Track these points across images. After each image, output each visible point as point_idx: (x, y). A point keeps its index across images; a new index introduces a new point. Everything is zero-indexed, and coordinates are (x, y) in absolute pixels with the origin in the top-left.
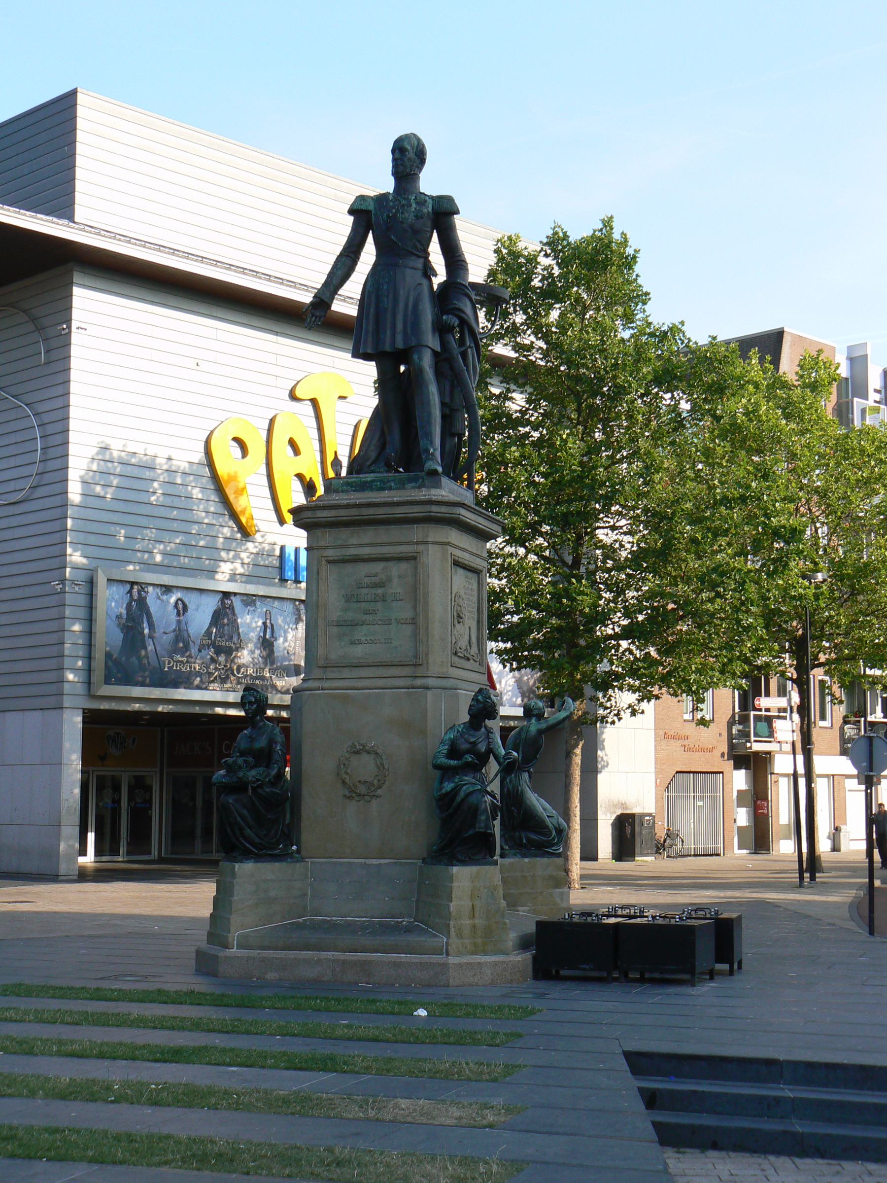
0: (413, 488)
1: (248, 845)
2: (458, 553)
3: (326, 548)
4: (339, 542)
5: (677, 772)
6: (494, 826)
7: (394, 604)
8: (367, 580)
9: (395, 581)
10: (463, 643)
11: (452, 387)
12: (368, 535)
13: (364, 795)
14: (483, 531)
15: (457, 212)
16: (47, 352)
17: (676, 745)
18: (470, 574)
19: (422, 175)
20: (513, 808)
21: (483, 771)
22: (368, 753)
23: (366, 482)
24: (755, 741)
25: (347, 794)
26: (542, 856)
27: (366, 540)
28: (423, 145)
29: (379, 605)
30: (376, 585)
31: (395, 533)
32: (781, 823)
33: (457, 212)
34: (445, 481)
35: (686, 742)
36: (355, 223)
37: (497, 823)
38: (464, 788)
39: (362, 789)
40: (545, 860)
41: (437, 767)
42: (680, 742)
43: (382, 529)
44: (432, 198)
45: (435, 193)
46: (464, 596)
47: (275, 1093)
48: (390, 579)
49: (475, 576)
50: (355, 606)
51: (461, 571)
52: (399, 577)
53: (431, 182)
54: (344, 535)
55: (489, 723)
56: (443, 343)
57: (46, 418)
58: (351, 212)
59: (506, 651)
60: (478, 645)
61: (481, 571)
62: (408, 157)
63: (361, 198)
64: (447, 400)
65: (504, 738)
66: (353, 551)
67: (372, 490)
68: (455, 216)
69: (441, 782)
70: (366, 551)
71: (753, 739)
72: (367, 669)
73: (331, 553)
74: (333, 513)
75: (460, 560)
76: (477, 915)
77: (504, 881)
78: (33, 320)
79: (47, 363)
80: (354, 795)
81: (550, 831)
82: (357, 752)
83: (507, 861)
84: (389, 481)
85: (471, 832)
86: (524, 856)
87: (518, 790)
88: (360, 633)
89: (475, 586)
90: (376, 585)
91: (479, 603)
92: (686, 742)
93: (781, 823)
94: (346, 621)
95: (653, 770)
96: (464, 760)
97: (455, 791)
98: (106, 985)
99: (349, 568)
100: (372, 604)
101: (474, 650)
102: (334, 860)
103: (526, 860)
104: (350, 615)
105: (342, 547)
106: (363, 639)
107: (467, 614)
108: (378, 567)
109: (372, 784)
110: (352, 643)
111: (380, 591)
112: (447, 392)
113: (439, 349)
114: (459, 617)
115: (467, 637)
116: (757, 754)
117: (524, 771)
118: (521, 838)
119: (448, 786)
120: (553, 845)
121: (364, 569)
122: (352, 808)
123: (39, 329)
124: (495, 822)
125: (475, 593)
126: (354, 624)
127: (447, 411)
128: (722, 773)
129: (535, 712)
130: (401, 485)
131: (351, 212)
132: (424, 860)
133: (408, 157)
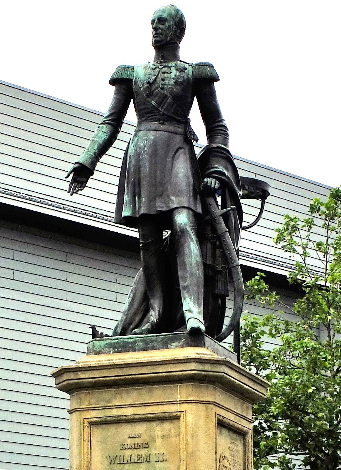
0: (176, 347)
2: (223, 413)
4: (102, 404)
8: (129, 442)
9: (159, 442)
14: (248, 391)
15: (217, 79)
23: (128, 343)
27: (129, 402)
30: (138, 447)
31: (159, 394)
32: (258, 273)
33: (217, 79)
34: (208, 340)
36: (117, 92)
43: (145, 390)
47: (181, 343)
48: (153, 439)
49: (239, 438)
51: (225, 432)
52: (164, 437)
54: (106, 395)
56: (206, 207)
58: (113, 82)
59: (221, 251)
61: (247, 433)
62: (169, 33)
64: (209, 262)
66: (115, 412)
67: (134, 350)
68: (215, 84)
70: (129, 412)
73: (93, 415)
74: (96, 374)
75: (225, 420)
84: (152, 341)
90: (138, 447)
93: (258, 273)
99: (112, 429)
105: (104, 408)
108: (141, 428)
111: (143, 452)
112: (209, 253)
113: (199, 210)
121: (127, 430)
125: (241, 454)
127: (210, 272)
130: (165, 345)
133: (169, 33)
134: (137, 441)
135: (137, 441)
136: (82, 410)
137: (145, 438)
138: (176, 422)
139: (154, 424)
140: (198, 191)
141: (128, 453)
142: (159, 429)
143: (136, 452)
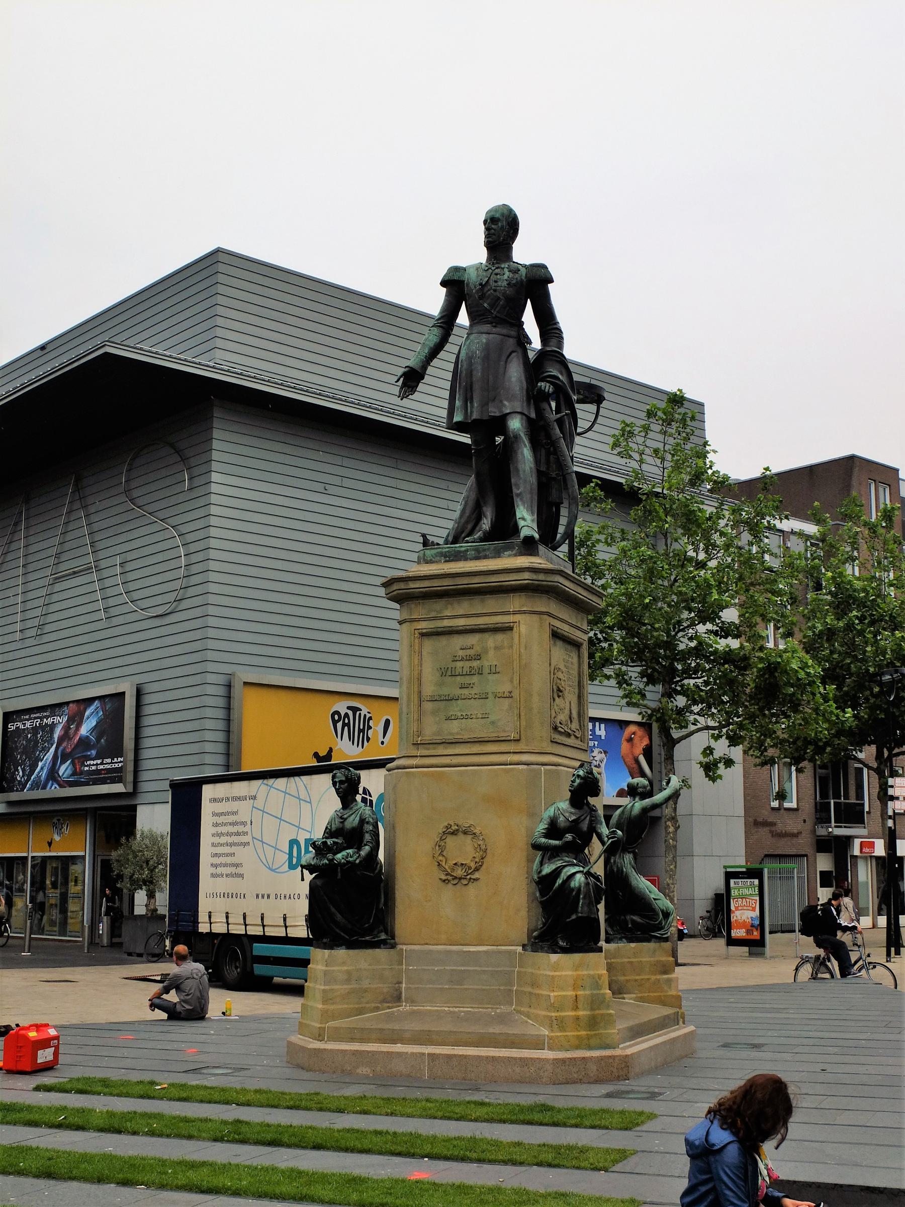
0: (509, 556)
1: (338, 931)
2: (557, 624)
3: (418, 620)
4: (433, 614)
5: (766, 856)
6: (598, 910)
7: (491, 677)
8: (461, 653)
9: (491, 653)
10: (563, 717)
11: (548, 454)
12: (464, 606)
13: (460, 879)
15: (551, 281)
16: (190, 479)
17: (764, 831)
18: (569, 647)
19: (515, 246)
20: (616, 888)
21: (586, 851)
22: (465, 833)
23: (460, 552)
24: (836, 827)
25: (444, 877)
26: (649, 941)
27: (461, 612)
28: (515, 215)
29: (475, 679)
31: (492, 604)
33: (551, 281)
34: (542, 549)
35: (773, 829)
36: (448, 295)
37: (601, 907)
38: (565, 870)
39: (459, 872)
40: (652, 945)
41: (536, 847)
42: (766, 829)
43: (477, 600)
44: (525, 266)
45: (528, 262)
46: (564, 669)
48: (486, 651)
49: (574, 649)
50: (448, 679)
51: (559, 643)
52: (496, 648)
53: (524, 252)
55: (592, 800)
56: (539, 412)
57: (190, 538)
58: (444, 283)
60: (580, 722)
61: (582, 644)
62: (501, 229)
63: (456, 269)
64: (543, 468)
65: (608, 818)
66: (446, 623)
67: (466, 559)
69: (542, 863)
70: (461, 622)
71: (833, 824)
72: (463, 745)
76: (580, 1006)
77: (610, 968)
78: (178, 452)
79: (190, 489)
80: (450, 878)
81: (658, 915)
82: (454, 833)
83: (612, 946)
84: (484, 550)
85: (574, 917)
86: (631, 940)
87: (622, 870)
88: (455, 709)
89: (575, 660)
91: (579, 675)
92: (773, 829)
94: (440, 696)
95: (744, 854)
96: (565, 839)
97: (557, 873)
98: (193, 1080)
99: (443, 641)
100: (467, 677)
101: (575, 726)
102: (431, 947)
103: (633, 945)
104: (445, 691)
106: (459, 714)
107: (568, 688)
108: (472, 640)
109: (470, 868)
110: (448, 719)
111: (475, 664)
112: (543, 460)
113: (533, 415)
114: (559, 690)
115: (567, 712)
116: (838, 837)
117: (629, 852)
118: (626, 922)
119: (547, 869)
120: (662, 928)
121: (458, 642)
122: (448, 892)
123: (183, 460)
124: (599, 906)
125: (576, 666)
126: (450, 699)
127: (544, 480)
128: (806, 855)
129: (640, 790)
130: (497, 554)
131: (444, 283)
132: (524, 946)
133: (501, 229)
134: (469, 652)
135: (469, 652)
136: (412, 621)
137: (478, 649)
138: (509, 633)
139: (486, 635)
140: (574, 917)
141: (459, 664)
142: (491, 641)
143: (468, 664)
